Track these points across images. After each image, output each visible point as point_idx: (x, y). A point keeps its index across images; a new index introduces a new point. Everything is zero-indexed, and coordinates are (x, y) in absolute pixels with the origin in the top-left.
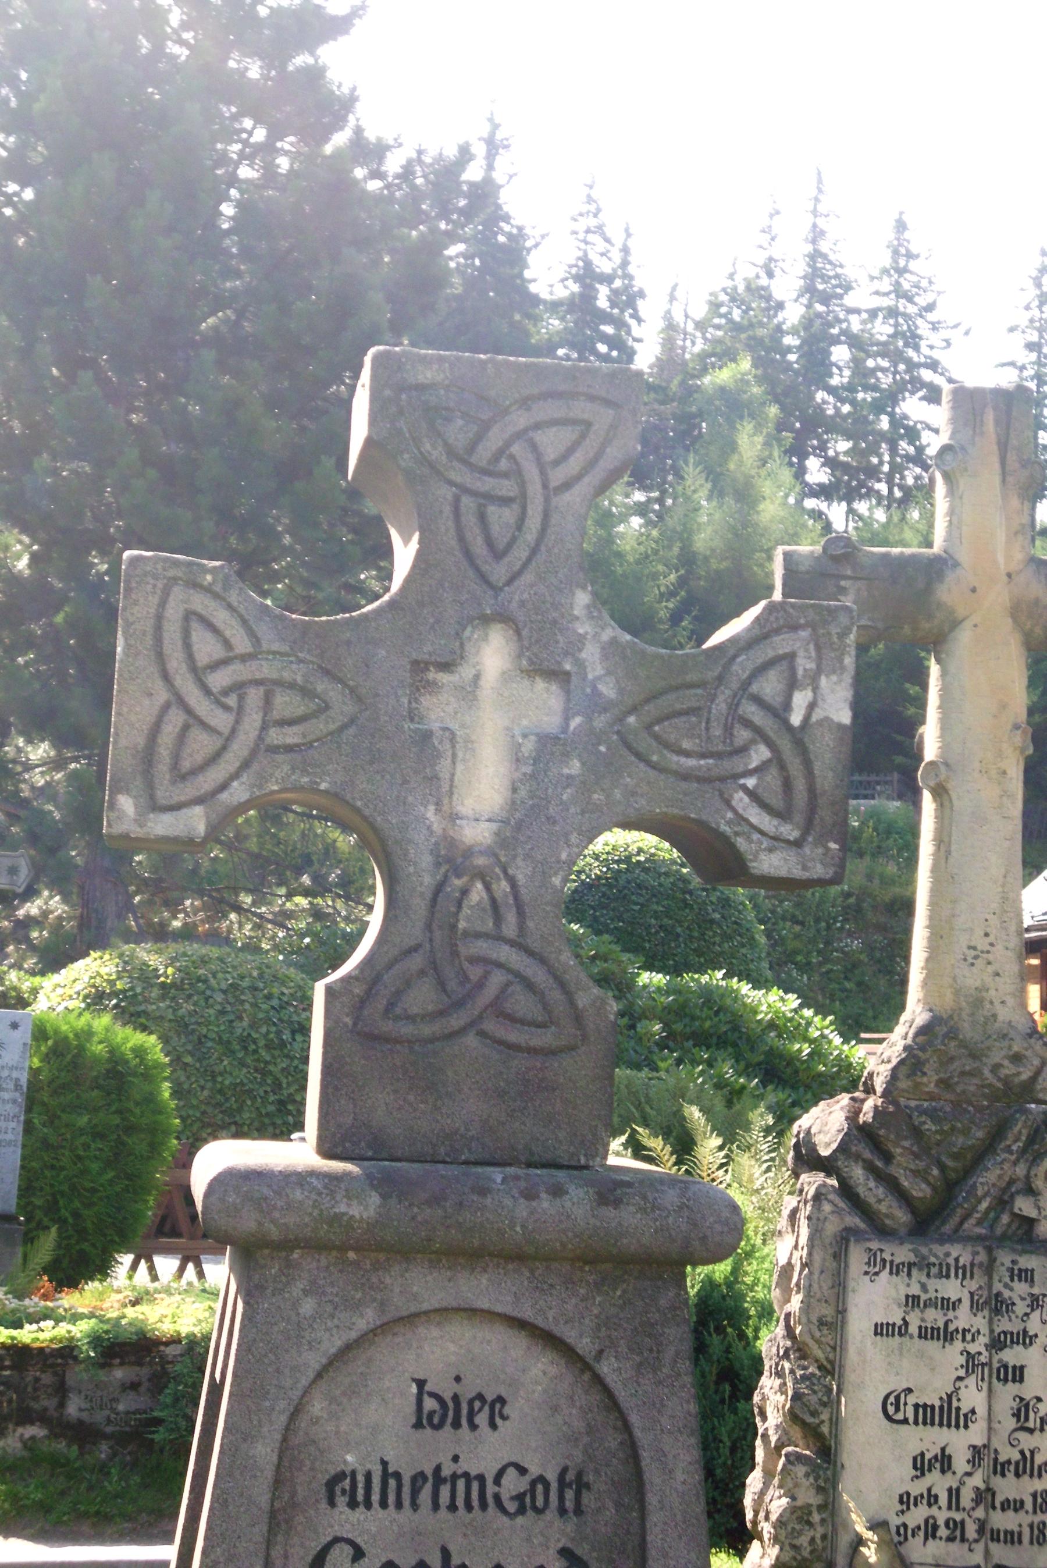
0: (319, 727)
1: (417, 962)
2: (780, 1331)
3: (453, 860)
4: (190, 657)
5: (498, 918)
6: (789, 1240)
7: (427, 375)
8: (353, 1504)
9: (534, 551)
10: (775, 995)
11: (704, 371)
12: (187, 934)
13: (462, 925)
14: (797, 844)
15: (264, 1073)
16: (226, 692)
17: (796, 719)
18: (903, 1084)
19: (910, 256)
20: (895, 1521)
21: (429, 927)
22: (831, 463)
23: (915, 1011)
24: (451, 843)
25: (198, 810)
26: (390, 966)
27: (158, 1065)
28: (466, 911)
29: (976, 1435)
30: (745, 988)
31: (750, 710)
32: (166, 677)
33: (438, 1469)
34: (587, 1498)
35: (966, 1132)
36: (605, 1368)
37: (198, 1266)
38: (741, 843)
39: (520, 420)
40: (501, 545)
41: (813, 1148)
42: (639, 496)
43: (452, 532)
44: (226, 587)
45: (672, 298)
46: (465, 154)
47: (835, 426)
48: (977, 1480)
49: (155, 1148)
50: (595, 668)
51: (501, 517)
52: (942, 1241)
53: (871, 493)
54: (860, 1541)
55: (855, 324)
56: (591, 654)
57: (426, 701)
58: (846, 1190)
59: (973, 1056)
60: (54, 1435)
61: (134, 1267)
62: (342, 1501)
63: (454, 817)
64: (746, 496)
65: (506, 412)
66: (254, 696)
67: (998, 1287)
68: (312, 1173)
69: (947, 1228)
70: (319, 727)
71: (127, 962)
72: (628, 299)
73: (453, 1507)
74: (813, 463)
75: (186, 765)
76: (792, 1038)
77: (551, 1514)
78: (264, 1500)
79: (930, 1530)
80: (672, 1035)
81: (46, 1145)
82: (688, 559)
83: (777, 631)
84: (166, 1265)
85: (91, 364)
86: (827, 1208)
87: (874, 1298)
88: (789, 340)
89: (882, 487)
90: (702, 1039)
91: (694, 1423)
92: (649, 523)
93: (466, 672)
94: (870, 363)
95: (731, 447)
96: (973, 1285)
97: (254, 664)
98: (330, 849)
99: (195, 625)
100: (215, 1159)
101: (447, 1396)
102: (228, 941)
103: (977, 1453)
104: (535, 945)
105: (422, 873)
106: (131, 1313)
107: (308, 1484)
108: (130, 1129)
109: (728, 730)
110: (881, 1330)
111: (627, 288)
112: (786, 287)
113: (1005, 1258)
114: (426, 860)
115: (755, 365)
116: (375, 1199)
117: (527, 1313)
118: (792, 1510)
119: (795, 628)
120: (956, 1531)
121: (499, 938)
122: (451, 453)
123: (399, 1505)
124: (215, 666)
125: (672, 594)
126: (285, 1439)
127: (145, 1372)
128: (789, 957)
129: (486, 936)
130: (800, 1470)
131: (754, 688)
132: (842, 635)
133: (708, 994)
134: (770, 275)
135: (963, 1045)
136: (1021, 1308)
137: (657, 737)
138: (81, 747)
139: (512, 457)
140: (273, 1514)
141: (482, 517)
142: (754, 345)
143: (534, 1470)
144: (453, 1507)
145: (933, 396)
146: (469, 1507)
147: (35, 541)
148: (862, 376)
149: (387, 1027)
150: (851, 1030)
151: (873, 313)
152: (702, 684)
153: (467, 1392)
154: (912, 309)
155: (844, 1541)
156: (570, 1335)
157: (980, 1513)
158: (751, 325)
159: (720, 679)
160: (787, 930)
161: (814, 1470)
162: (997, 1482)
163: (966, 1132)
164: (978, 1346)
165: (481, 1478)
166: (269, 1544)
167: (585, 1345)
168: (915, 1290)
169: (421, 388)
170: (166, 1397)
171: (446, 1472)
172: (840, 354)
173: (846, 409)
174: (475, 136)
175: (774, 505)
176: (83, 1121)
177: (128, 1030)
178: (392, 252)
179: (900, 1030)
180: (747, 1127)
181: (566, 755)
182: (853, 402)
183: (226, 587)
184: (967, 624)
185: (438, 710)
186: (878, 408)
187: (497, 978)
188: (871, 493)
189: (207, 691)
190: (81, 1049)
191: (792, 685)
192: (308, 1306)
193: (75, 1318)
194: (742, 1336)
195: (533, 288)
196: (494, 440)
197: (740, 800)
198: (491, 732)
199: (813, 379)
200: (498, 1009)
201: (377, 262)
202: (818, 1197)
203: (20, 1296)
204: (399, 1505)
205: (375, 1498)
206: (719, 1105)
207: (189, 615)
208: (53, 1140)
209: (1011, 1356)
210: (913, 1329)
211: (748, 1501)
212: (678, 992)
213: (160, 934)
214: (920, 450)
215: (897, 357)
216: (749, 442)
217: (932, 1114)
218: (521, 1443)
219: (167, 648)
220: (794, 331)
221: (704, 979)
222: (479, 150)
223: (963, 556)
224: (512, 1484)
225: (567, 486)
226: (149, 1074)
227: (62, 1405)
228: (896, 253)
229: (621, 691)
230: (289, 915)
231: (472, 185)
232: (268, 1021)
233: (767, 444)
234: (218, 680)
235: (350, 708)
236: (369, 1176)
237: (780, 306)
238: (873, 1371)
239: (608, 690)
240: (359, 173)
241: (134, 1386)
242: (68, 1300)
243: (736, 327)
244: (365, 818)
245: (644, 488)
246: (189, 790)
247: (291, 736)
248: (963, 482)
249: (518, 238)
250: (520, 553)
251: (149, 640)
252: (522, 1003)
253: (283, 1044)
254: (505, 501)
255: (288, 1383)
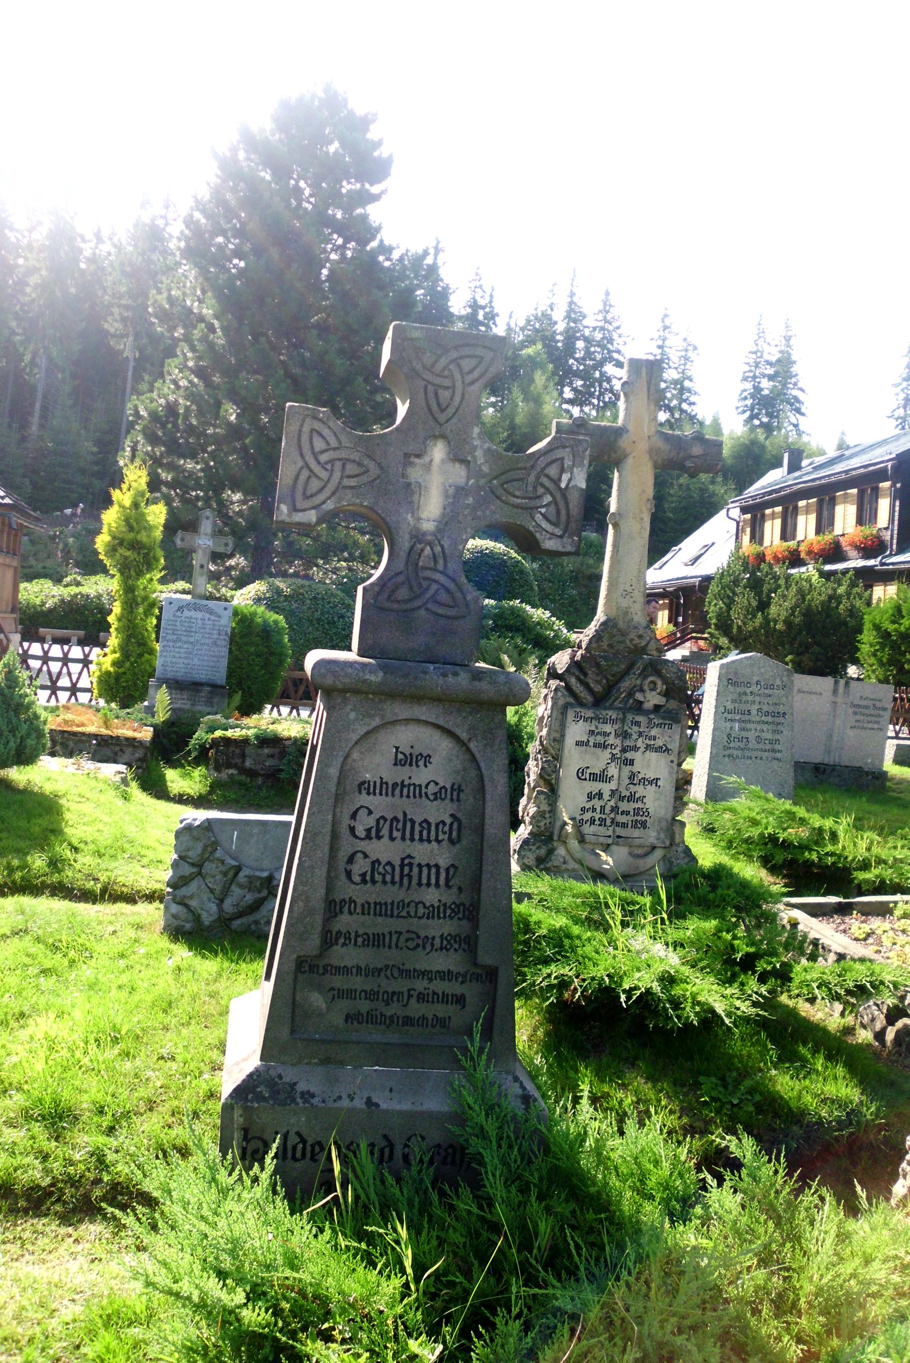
0: (365, 479)
1: (401, 578)
2: (538, 743)
3: (418, 537)
4: (312, 448)
5: (436, 562)
6: (543, 706)
7: (416, 334)
8: (368, 793)
9: (457, 410)
10: (540, 611)
11: (522, 349)
12: (296, 575)
13: (420, 564)
14: (561, 537)
15: (326, 634)
16: (326, 463)
17: (563, 485)
18: (594, 645)
19: (610, 306)
20: (579, 818)
21: (407, 564)
22: (574, 390)
23: (600, 616)
24: (418, 530)
25: (313, 512)
26: (390, 580)
27: (283, 628)
28: (422, 558)
29: (613, 785)
30: (528, 608)
31: (544, 480)
32: (302, 455)
33: (403, 782)
34: (462, 795)
35: (618, 666)
36: (472, 745)
37: (298, 711)
38: (538, 535)
39: (454, 354)
40: (444, 407)
41: (555, 670)
42: (493, 399)
43: (424, 401)
44: (328, 418)
45: (510, 317)
46: (426, 253)
47: (577, 374)
48: (612, 803)
49: (281, 662)
50: (481, 460)
51: (444, 395)
52: (606, 709)
53: (590, 403)
54: (565, 824)
55: (587, 332)
56: (479, 453)
57: (409, 470)
58: (568, 688)
59: (623, 635)
60: (240, 773)
61: (272, 709)
62: (364, 792)
63: (419, 519)
64: (537, 401)
65: (448, 351)
66: (338, 465)
67: (626, 728)
68: (356, 662)
69: (608, 704)
70: (365, 479)
71: (271, 585)
72: (491, 316)
73: (408, 796)
74: (567, 389)
75: (309, 493)
76: (546, 629)
77: (447, 801)
78: (333, 790)
79: (592, 821)
80: (496, 626)
81: (237, 659)
82: (512, 427)
83: (557, 448)
84: (285, 710)
85: (265, 335)
86: (560, 694)
87: (576, 731)
88: (559, 337)
89: (595, 401)
90: (509, 628)
91: (506, 768)
92: (496, 410)
93: (426, 459)
94: (592, 349)
95: (532, 381)
96: (616, 727)
97: (338, 452)
98: (356, 543)
99: (315, 434)
100: (313, 658)
101: (408, 753)
102: (312, 579)
103: (613, 792)
104: (451, 574)
105: (405, 543)
106: (271, 727)
107: (351, 785)
108: (272, 654)
109: (535, 488)
110: (578, 743)
111: (491, 312)
112: (559, 315)
113: (630, 717)
114: (407, 537)
115: (544, 347)
116: (381, 674)
117: (441, 722)
118: (538, 812)
119: (564, 447)
120: (602, 822)
121: (435, 570)
122: (424, 367)
123: (387, 795)
124: (322, 452)
125: (505, 441)
126: (342, 767)
127: (276, 751)
128: (547, 596)
129: (431, 569)
130: (542, 797)
131: (546, 471)
132: (584, 452)
133: (512, 608)
134: (552, 310)
135: (619, 630)
136: (635, 736)
137: (505, 490)
138: (254, 495)
139: (450, 370)
140: (337, 795)
141: (436, 394)
142: (544, 339)
143: (441, 784)
144: (408, 796)
145: (619, 365)
146: (415, 797)
147: (238, 408)
148: (588, 354)
149: (388, 605)
150: (571, 627)
151: (595, 329)
152: (525, 468)
153: (416, 752)
154: (611, 328)
155: (558, 824)
156: (458, 732)
157: (612, 815)
158: (543, 330)
159: (533, 467)
160: (546, 585)
161: (548, 797)
162: (620, 804)
163: (618, 666)
164: (616, 751)
165: (420, 786)
166: (335, 807)
167: (464, 736)
168: (593, 728)
169: (411, 339)
170: (285, 761)
171: (406, 783)
172: (580, 344)
173: (582, 367)
174: (431, 244)
175: (549, 405)
176: (252, 649)
177: (272, 613)
178: (394, 292)
179: (593, 623)
180: (527, 663)
181: (467, 495)
182: (585, 365)
183: (328, 418)
184: (631, 456)
185: (415, 474)
186: (595, 368)
187: (434, 587)
188: (590, 403)
189: (319, 463)
190: (252, 621)
191: (562, 471)
192: (352, 716)
193: (249, 728)
194: (521, 746)
195: (451, 310)
196: (443, 362)
197: (538, 517)
198: (435, 485)
199: (566, 355)
200: (434, 599)
201: (387, 295)
202: (556, 690)
203: (227, 718)
204: (387, 795)
205: (378, 791)
206: (515, 655)
207: (312, 430)
208: (240, 656)
209: (629, 755)
210: (591, 744)
211: (520, 809)
212: (500, 608)
213: (284, 575)
214: (612, 387)
215: (603, 347)
216: (540, 378)
217: (605, 658)
218: (437, 772)
219: (303, 444)
220: (561, 334)
221: (511, 603)
222: (432, 251)
223: (630, 427)
224: (432, 789)
225: (472, 383)
226: (279, 631)
227: (243, 762)
228: (605, 304)
229: (491, 469)
230: (339, 569)
231: (428, 265)
232: (328, 612)
233: (548, 380)
234: (324, 458)
235: (378, 472)
236: (379, 665)
237: (556, 323)
238: (574, 759)
239: (485, 469)
240: (381, 258)
241: (272, 756)
242: (246, 721)
243: (537, 331)
244: (382, 518)
245: (496, 396)
246: (309, 504)
247: (353, 482)
248: (631, 398)
249: (446, 288)
250: (451, 411)
251: (296, 441)
252: (443, 597)
253: (334, 623)
254: (447, 388)
255: (344, 745)
